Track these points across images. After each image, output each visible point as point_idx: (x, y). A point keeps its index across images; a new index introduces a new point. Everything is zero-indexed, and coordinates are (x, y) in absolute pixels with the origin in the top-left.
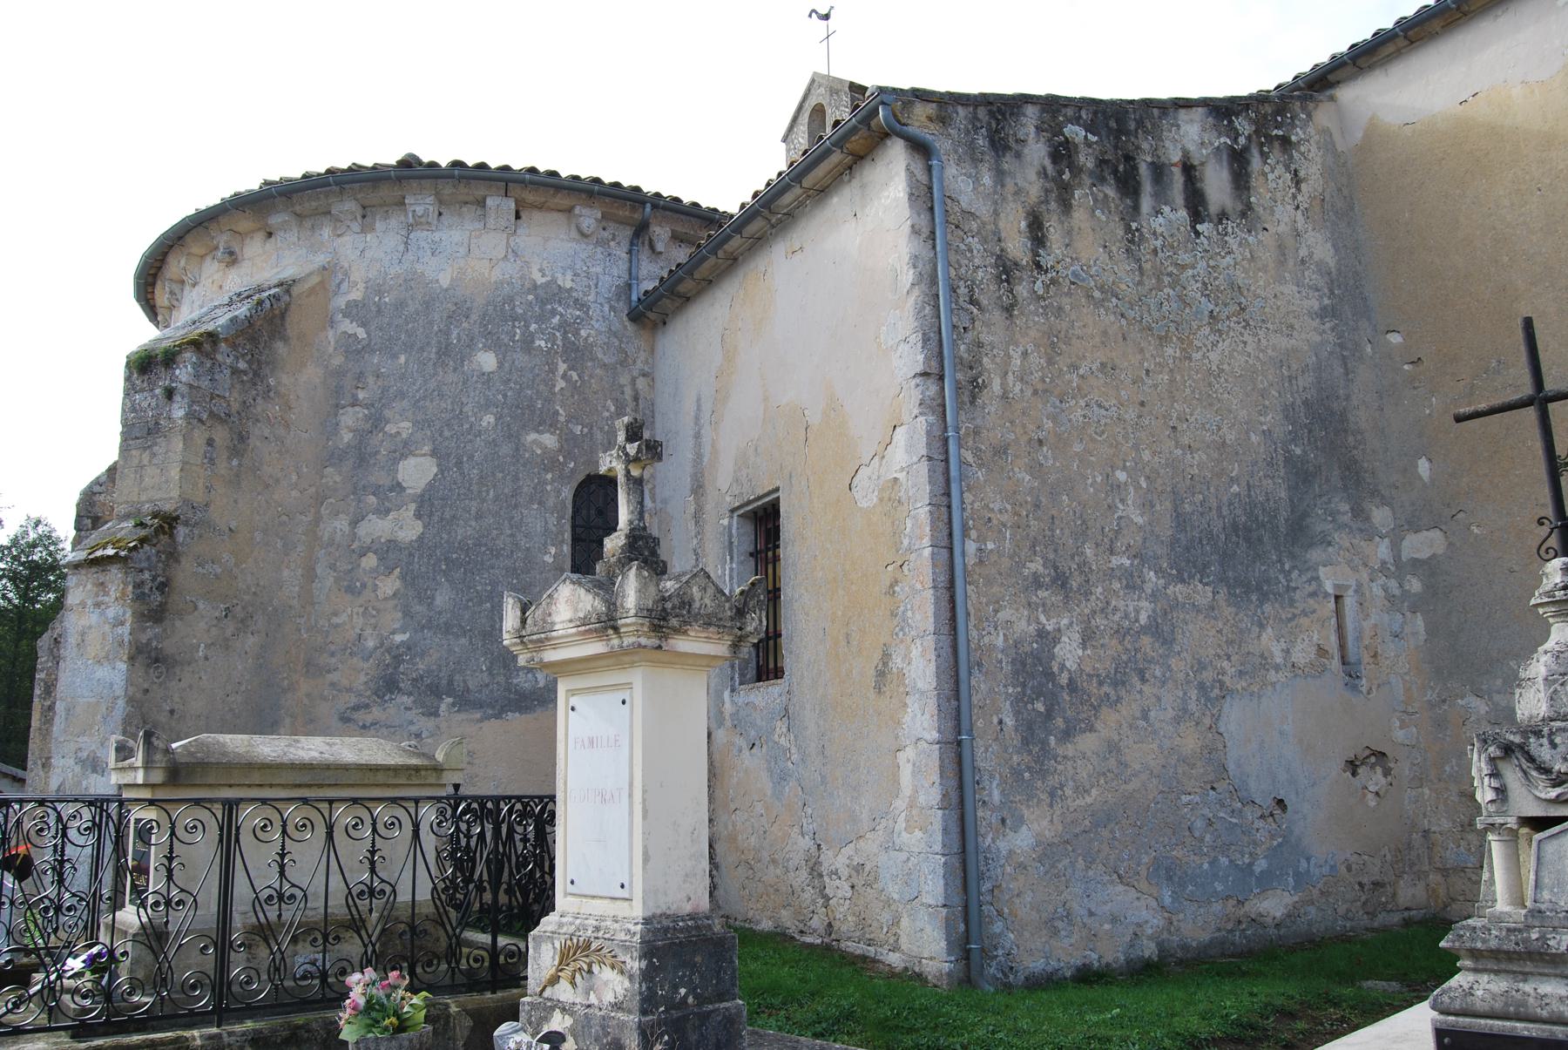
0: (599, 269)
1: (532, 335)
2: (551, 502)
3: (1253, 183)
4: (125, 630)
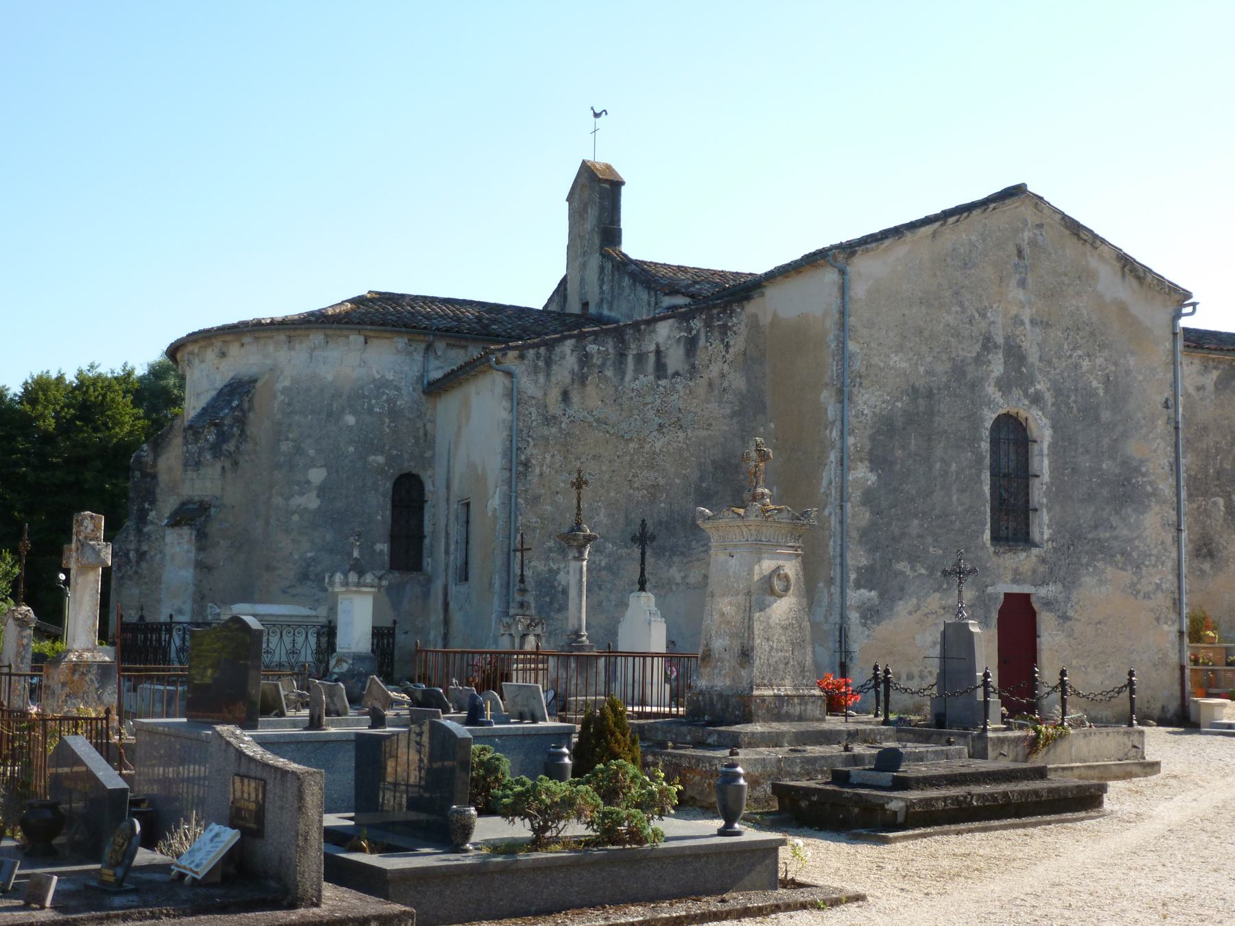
0: (407, 368)
1: (373, 406)
2: (381, 489)
3: (698, 353)
4: (192, 555)
